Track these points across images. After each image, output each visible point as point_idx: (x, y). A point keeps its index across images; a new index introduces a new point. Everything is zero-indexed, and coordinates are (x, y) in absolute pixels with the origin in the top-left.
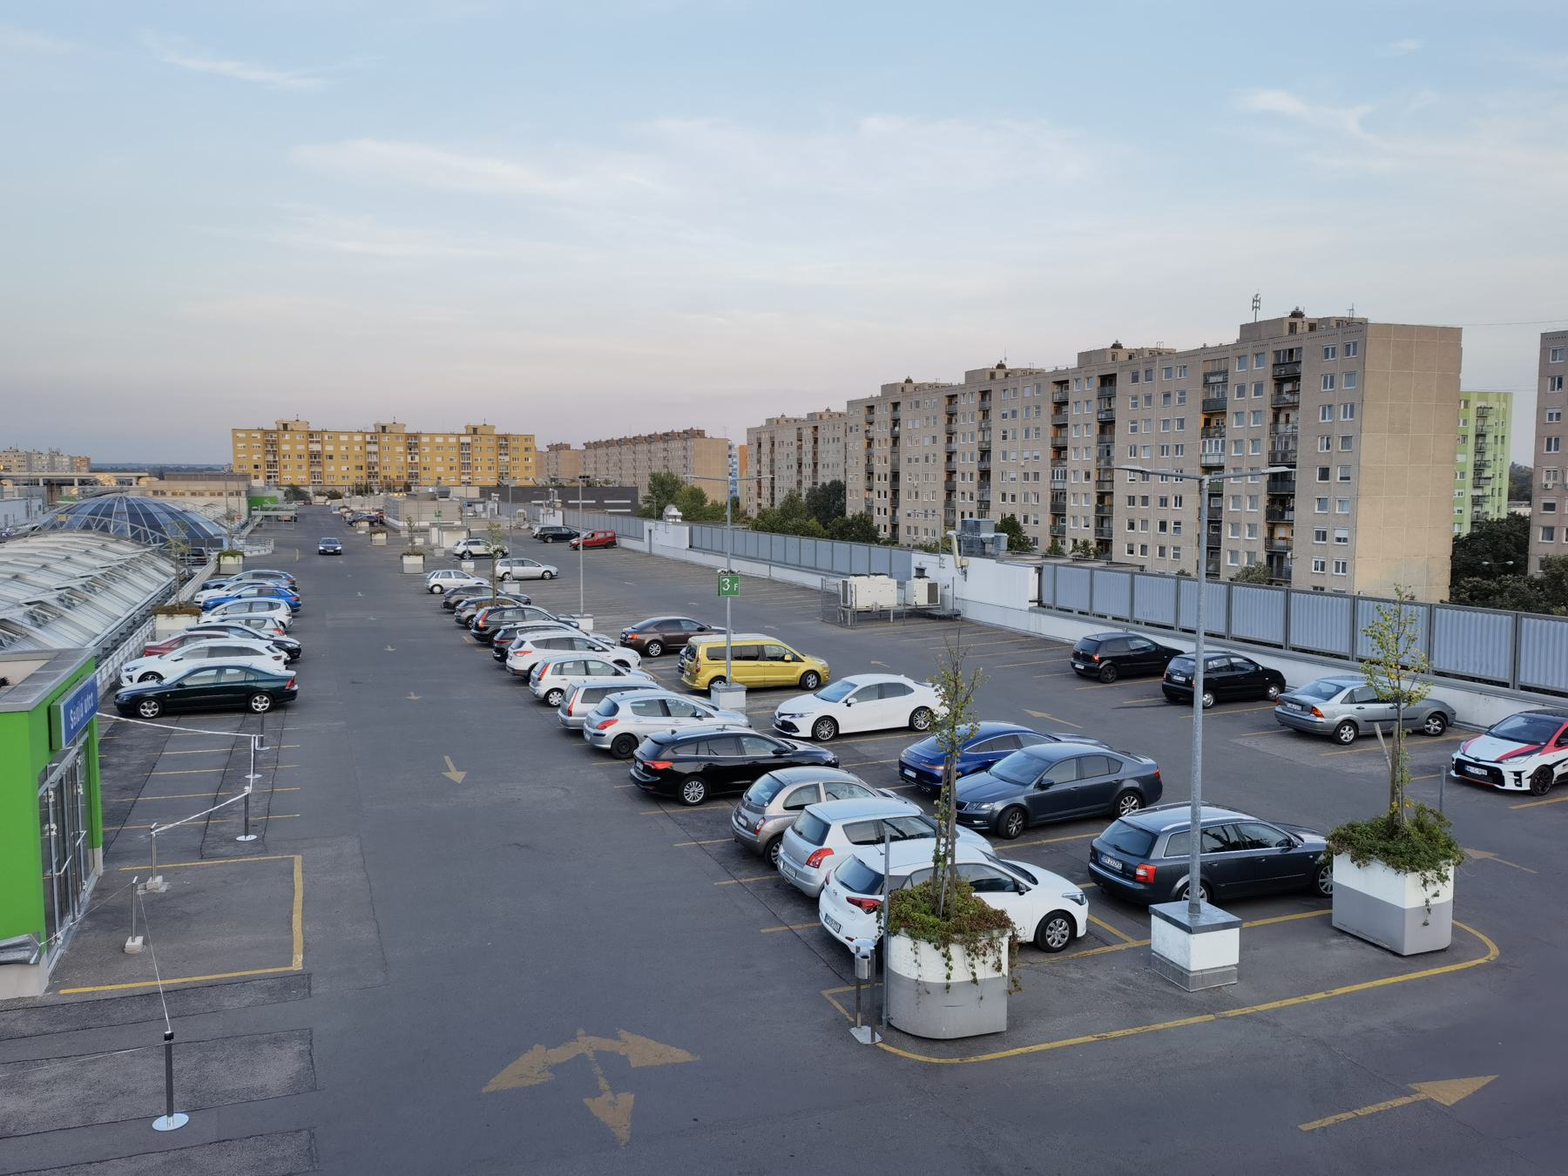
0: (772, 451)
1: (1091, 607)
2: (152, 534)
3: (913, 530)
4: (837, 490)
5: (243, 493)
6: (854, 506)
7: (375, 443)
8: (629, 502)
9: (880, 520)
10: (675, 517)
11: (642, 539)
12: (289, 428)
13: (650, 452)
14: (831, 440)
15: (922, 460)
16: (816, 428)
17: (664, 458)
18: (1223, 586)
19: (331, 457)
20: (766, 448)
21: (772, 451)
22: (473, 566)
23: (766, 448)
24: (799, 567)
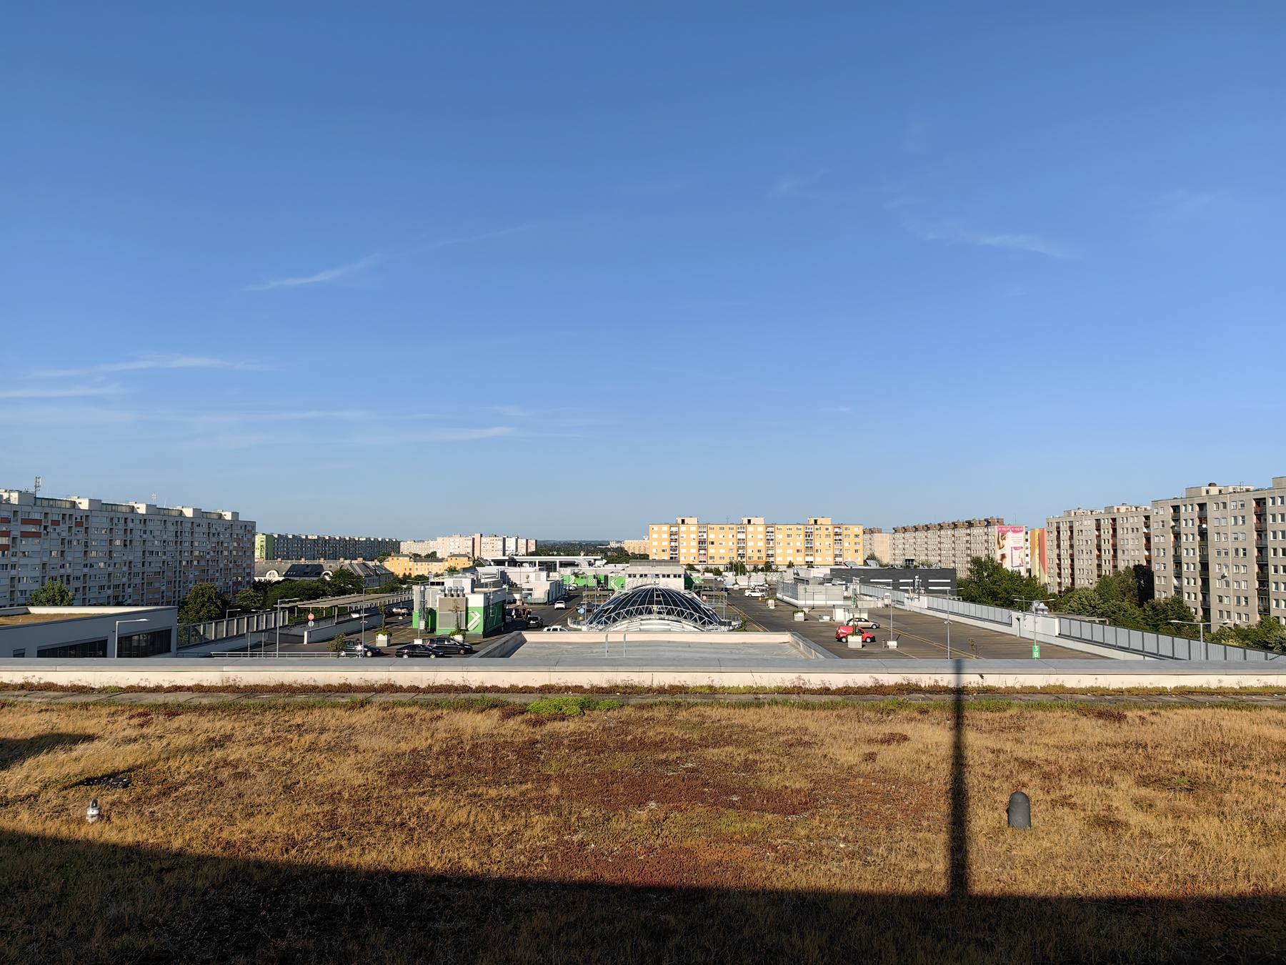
0: (1071, 538)
1: (1158, 652)
2: (676, 609)
3: (1225, 614)
4: (1144, 574)
5: (682, 576)
6: (1164, 588)
7: (743, 532)
8: (949, 581)
9: (1193, 601)
10: (1043, 610)
11: (1010, 625)
12: (686, 523)
13: (953, 536)
14: (1130, 530)
15: (1232, 553)
16: (1114, 520)
17: (967, 541)
18: (940, 864)
19: (713, 543)
20: (1065, 535)
21: (1071, 538)
22: (896, 645)
23: (1065, 535)
24: (1080, 640)
